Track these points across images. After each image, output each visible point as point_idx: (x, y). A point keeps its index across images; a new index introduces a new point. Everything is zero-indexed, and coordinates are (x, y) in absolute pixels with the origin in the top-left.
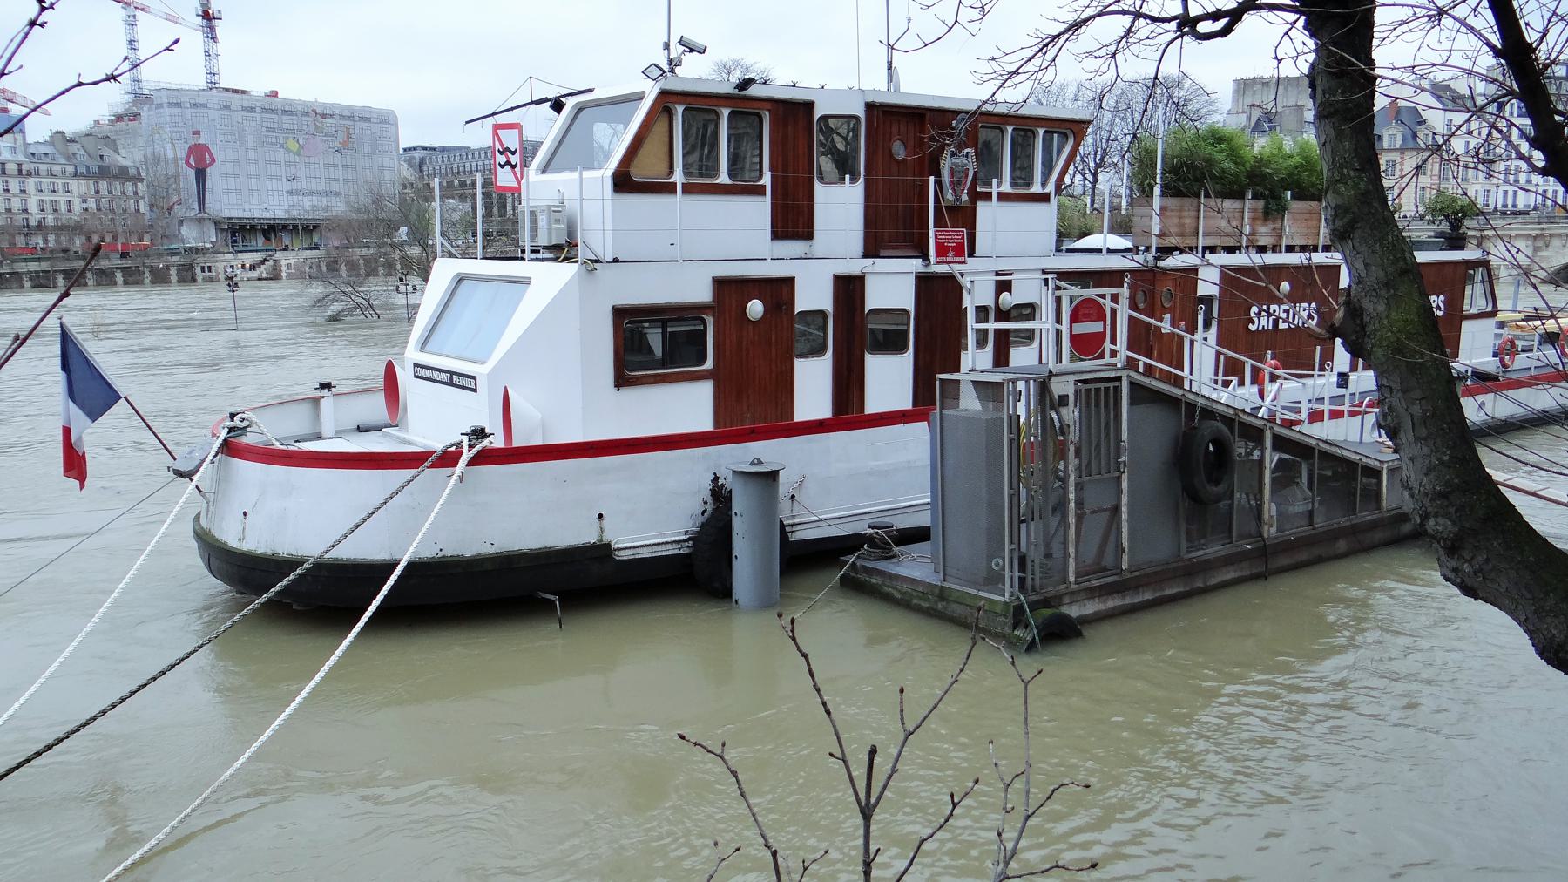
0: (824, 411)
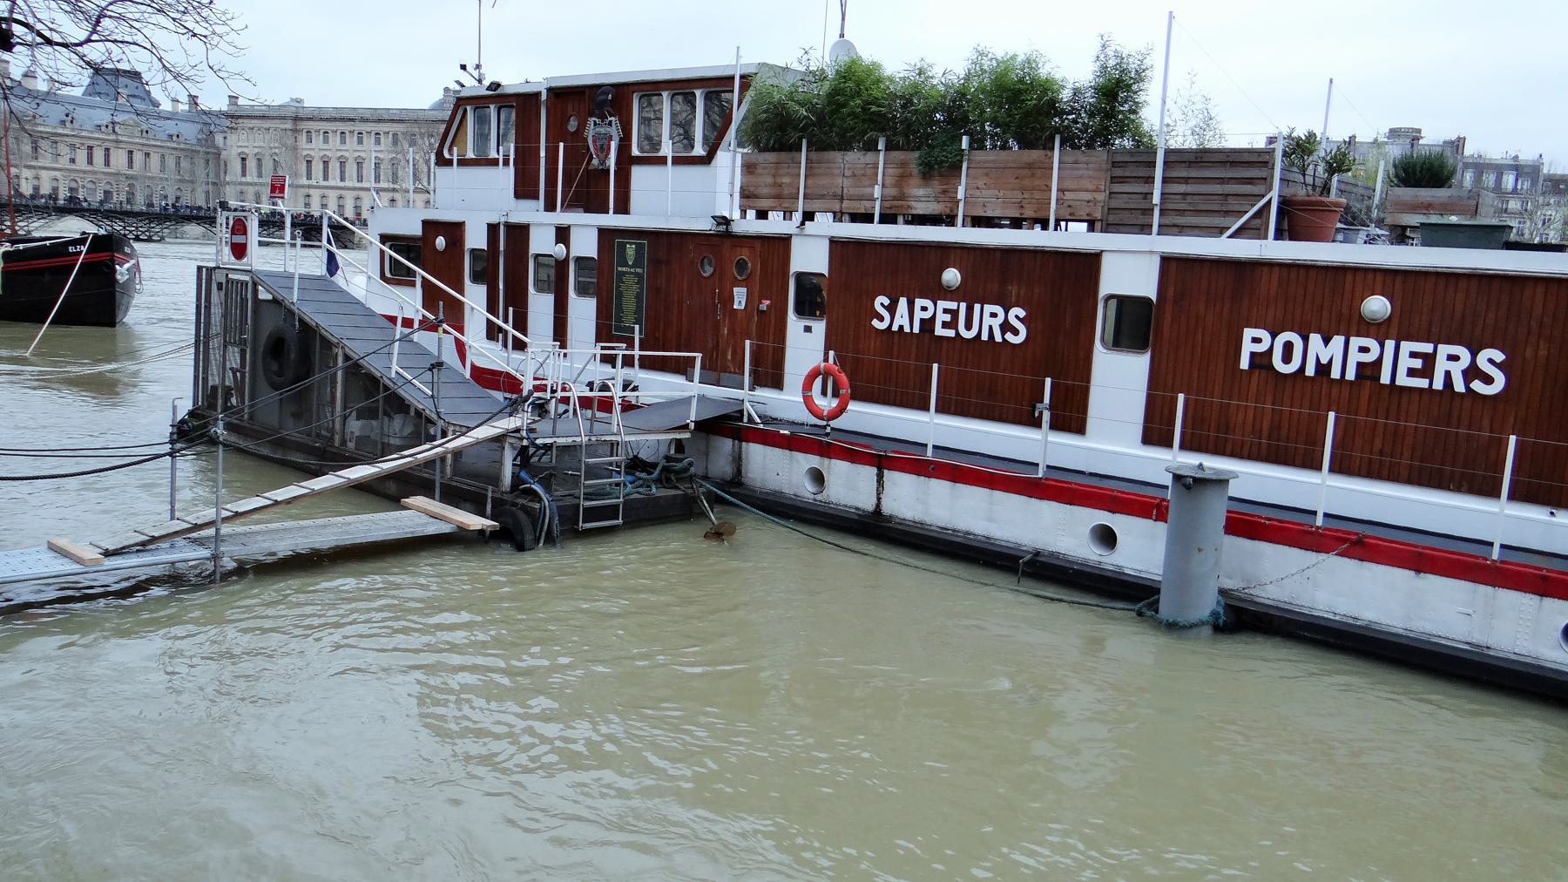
0: (1427, 381)
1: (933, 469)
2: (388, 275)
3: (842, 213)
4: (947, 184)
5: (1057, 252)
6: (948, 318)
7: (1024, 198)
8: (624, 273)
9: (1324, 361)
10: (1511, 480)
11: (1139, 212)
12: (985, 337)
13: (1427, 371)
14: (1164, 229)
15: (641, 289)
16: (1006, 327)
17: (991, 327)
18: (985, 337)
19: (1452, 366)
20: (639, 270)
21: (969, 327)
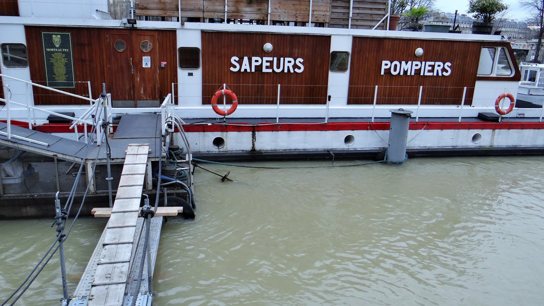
1: (280, 128)
3: (204, 18)
4: (261, 6)
5: (315, 35)
6: (268, 64)
7: (297, 13)
8: (53, 52)
9: (406, 70)
10: (277, 96)
11: (342, 20)
12: (286, 71)
13: (432, 71)
14: (354, 26)
15: (69, 60)
17: (288, 67)
18: (286, 71)
21: (278, 67)
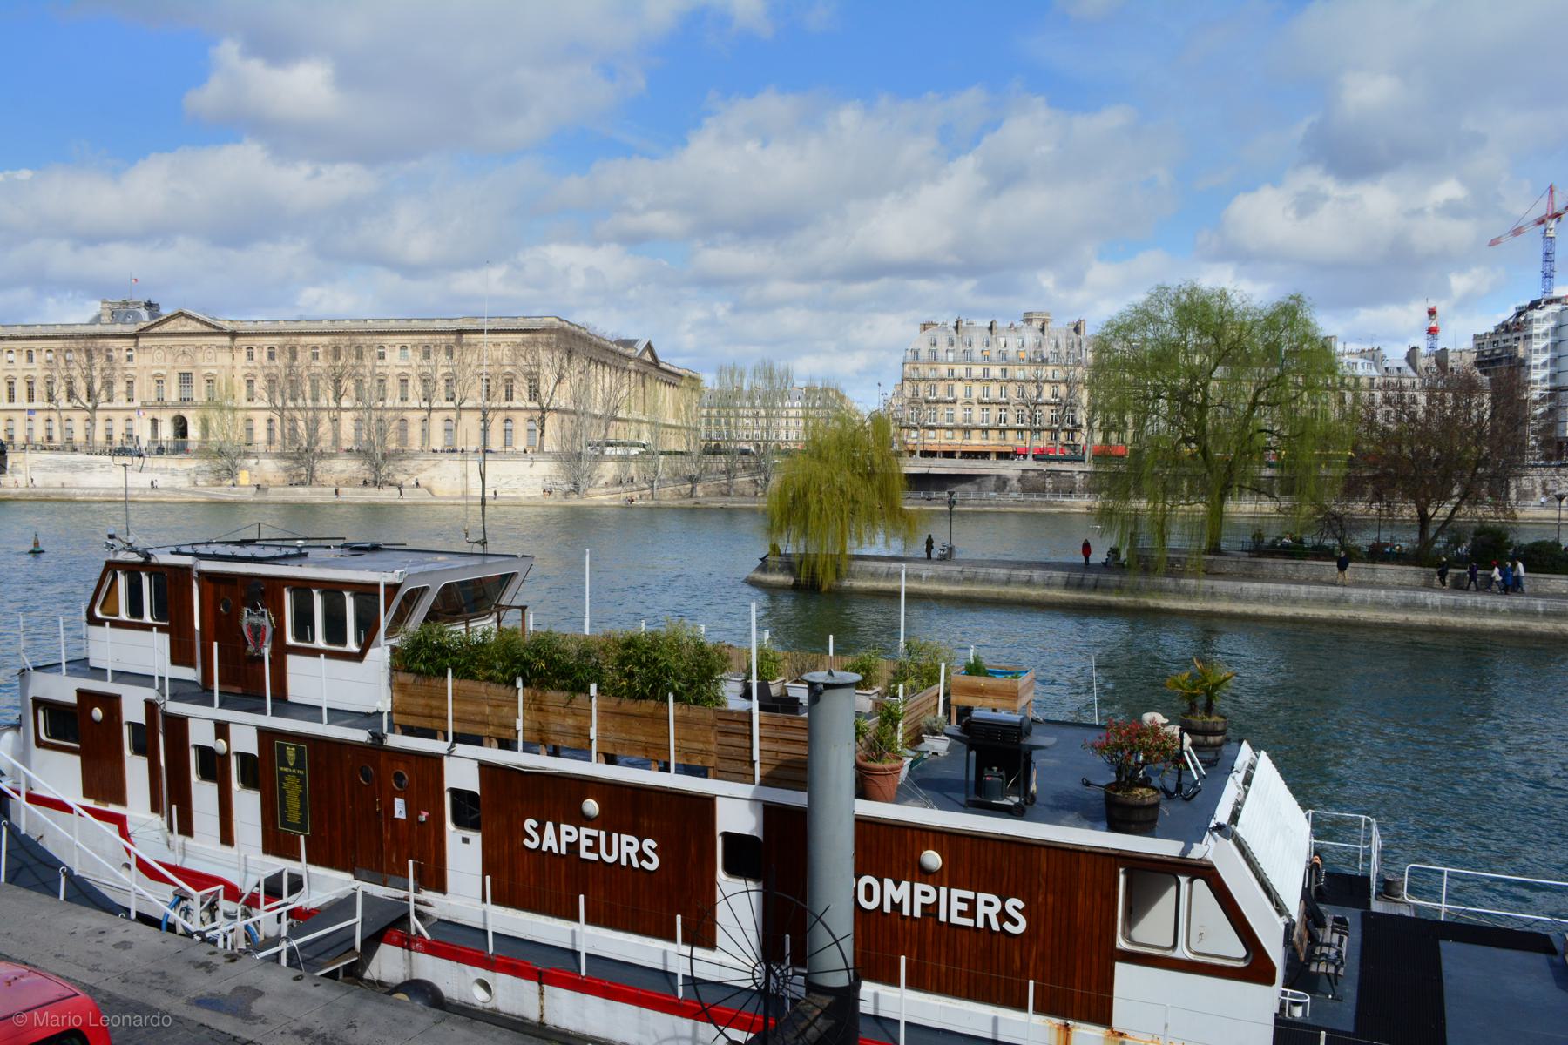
2: (43, 737)
6: (590, 843)
8: (286, 773)
9: (897, 901)
13: (972, 912)
15: (304, 789)
16: (641, 855)
17: (628, 855)
18: (624, 862)
19: (988, 910)
20: (300, 772)
21: (609, 852)
